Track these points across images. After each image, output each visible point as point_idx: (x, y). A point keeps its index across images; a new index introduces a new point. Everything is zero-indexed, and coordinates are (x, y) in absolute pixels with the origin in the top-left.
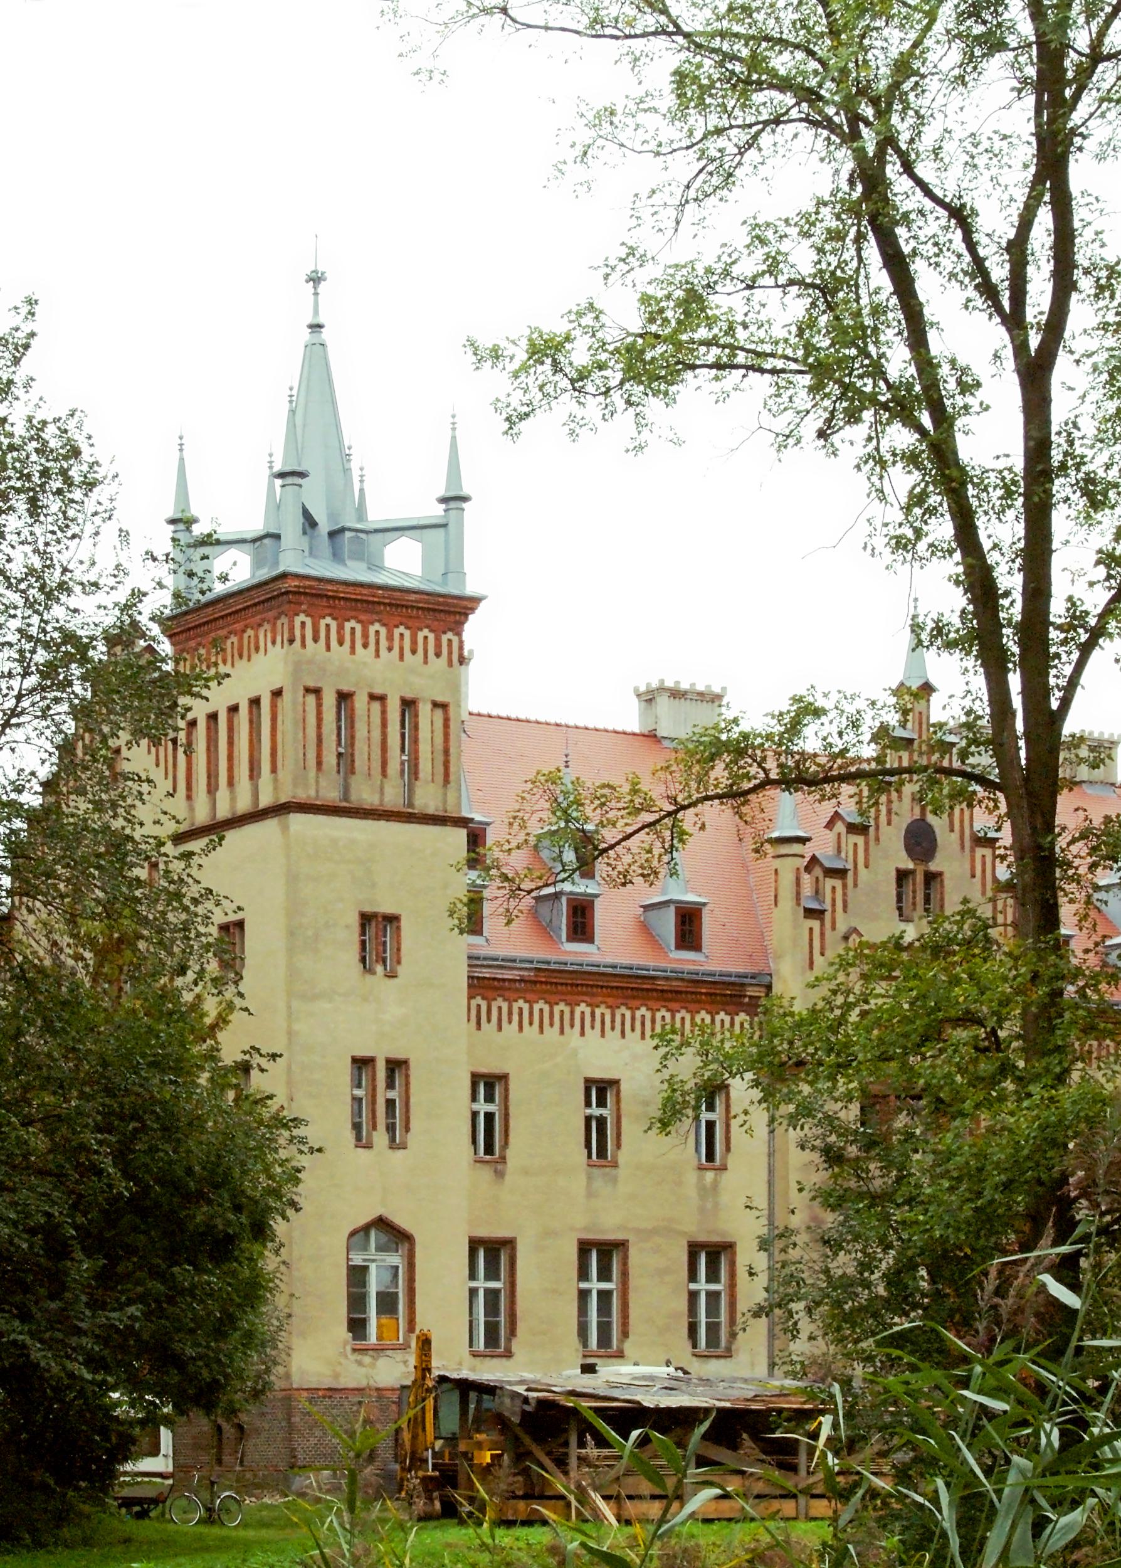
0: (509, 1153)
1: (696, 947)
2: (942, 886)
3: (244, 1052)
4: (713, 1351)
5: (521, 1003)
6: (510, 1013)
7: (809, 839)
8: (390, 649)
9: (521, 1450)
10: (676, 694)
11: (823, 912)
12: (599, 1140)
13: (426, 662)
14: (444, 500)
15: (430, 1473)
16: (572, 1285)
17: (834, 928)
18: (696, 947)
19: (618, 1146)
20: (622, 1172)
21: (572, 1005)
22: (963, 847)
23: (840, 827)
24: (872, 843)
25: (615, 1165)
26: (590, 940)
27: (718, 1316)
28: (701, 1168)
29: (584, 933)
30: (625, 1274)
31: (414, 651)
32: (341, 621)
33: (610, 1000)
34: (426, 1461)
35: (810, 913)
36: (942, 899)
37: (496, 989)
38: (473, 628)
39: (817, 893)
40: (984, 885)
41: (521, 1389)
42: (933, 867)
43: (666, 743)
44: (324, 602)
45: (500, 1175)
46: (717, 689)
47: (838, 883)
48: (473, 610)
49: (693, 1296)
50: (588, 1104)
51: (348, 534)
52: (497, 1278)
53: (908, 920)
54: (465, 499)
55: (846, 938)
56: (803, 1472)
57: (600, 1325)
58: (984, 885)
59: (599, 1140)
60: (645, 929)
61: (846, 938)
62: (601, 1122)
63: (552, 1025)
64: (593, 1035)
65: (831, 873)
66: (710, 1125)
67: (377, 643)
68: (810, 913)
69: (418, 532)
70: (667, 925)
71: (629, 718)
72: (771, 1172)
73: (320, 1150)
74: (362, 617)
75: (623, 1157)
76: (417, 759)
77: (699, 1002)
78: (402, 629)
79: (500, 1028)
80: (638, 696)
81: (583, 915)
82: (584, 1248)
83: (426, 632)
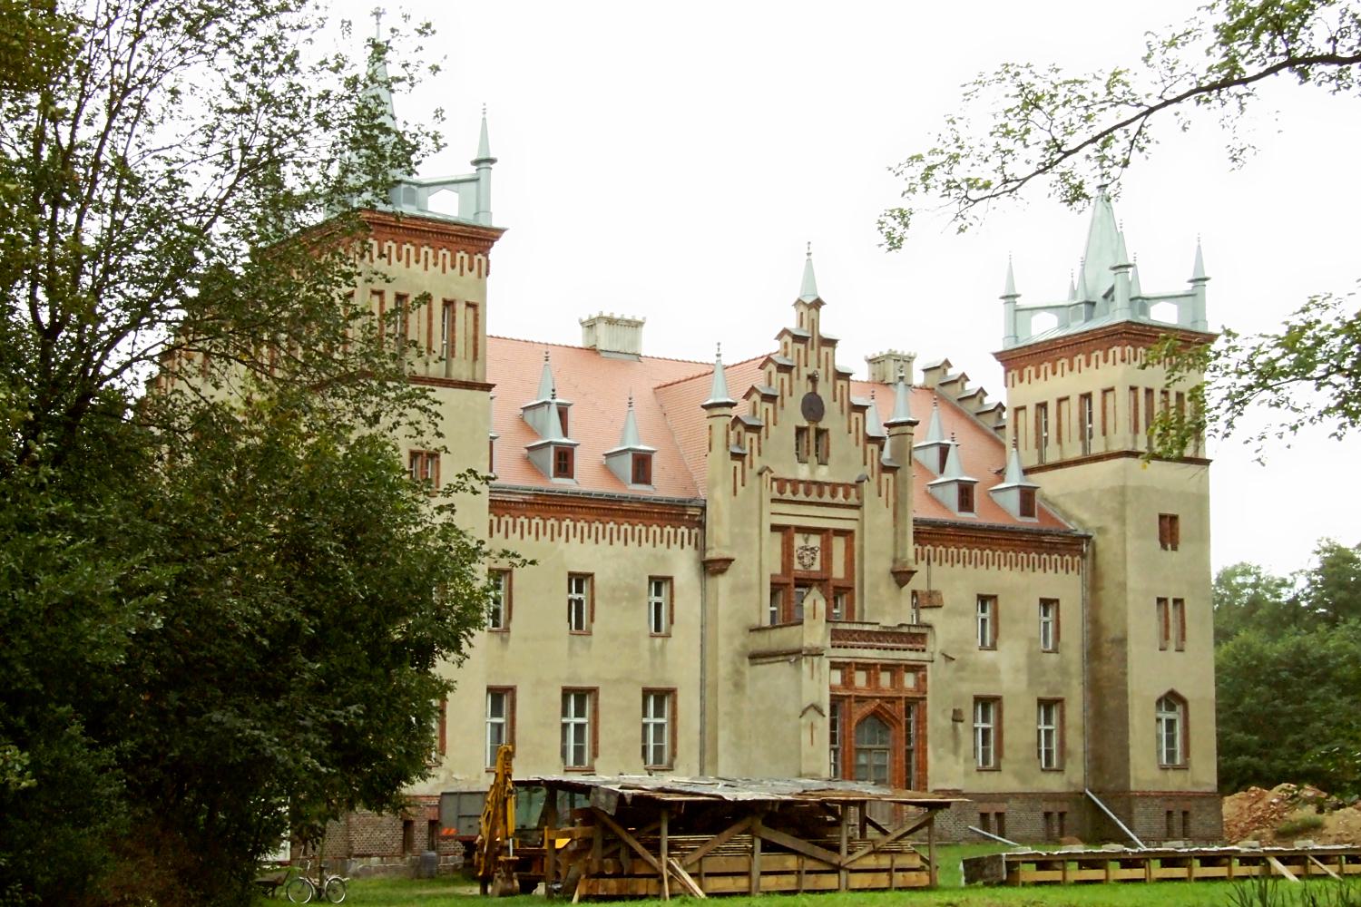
0: (512, 626)
1: (647, 481)
2: (828, 439)
3: (459, 476)
4: (657, 766)
5: (522, 519)
6: (514, 526)
7: (735, 405)
8: (435, 264)
9: (610, 837)
10: (611, 321)
11: (744, 455)
12: (578, 616)
13: (462, 274)
14: (477, 162)
15: (511, 858)
16: (558, 720)
17: (751, 467)
18: (647, 481)
19: (592, 620)
20: (595, 638)
21: (560, 520)
22: (842, 411)
23: (756, 397)
24: (778, 410)
25: (590, 633)
26: (571, 476)
27: (662, 741)
28: (652, 636)
29: (566, 470)
30: (595, 712)
31: (453, 267)
32: (400, 244)
33: (588, 517)
34: (508, 848)
35: (735, 456)
36: (828, 447)
37: (504, 508)
38: (496, 251)
39: (739, 443)
40: (857, 438)
41: (615, 788)
42: (822, 425)
43: (604, 354)
44: (388, 230)
45: (505, 641)
46: (639, 319)
47: (755, 436)
48: (498, 238)
49: (645, 726)
50: (570, 591)
51: (403, 186)
52: (500, 715)
53: (802, 461)
54: (492, 161)
55: (760, 474)
56: (844, 852)
57: (576, 748)
58: (857, 438)
59: (578, 616)
60: (607, 469)
61: (760, 474)
62: (579, 603)
63: (545, 534)
64: (575, 541)
65: (750, 428)
66: (658, 606)
67: (426, 260)
68: (735, 456)
69: (454, 186)
70: (627, 465)
71: (577, 338)
72: (702, 637)
73: (533, 562)
74: (416, 242)
75: (596, 627)
76: (453, 342)
77: (651, 518)
78: (444, 251)
79: (507, 536)
80: (582, 324)
81: (566, 459)
82: (566, 692)
83: (462, 253)
